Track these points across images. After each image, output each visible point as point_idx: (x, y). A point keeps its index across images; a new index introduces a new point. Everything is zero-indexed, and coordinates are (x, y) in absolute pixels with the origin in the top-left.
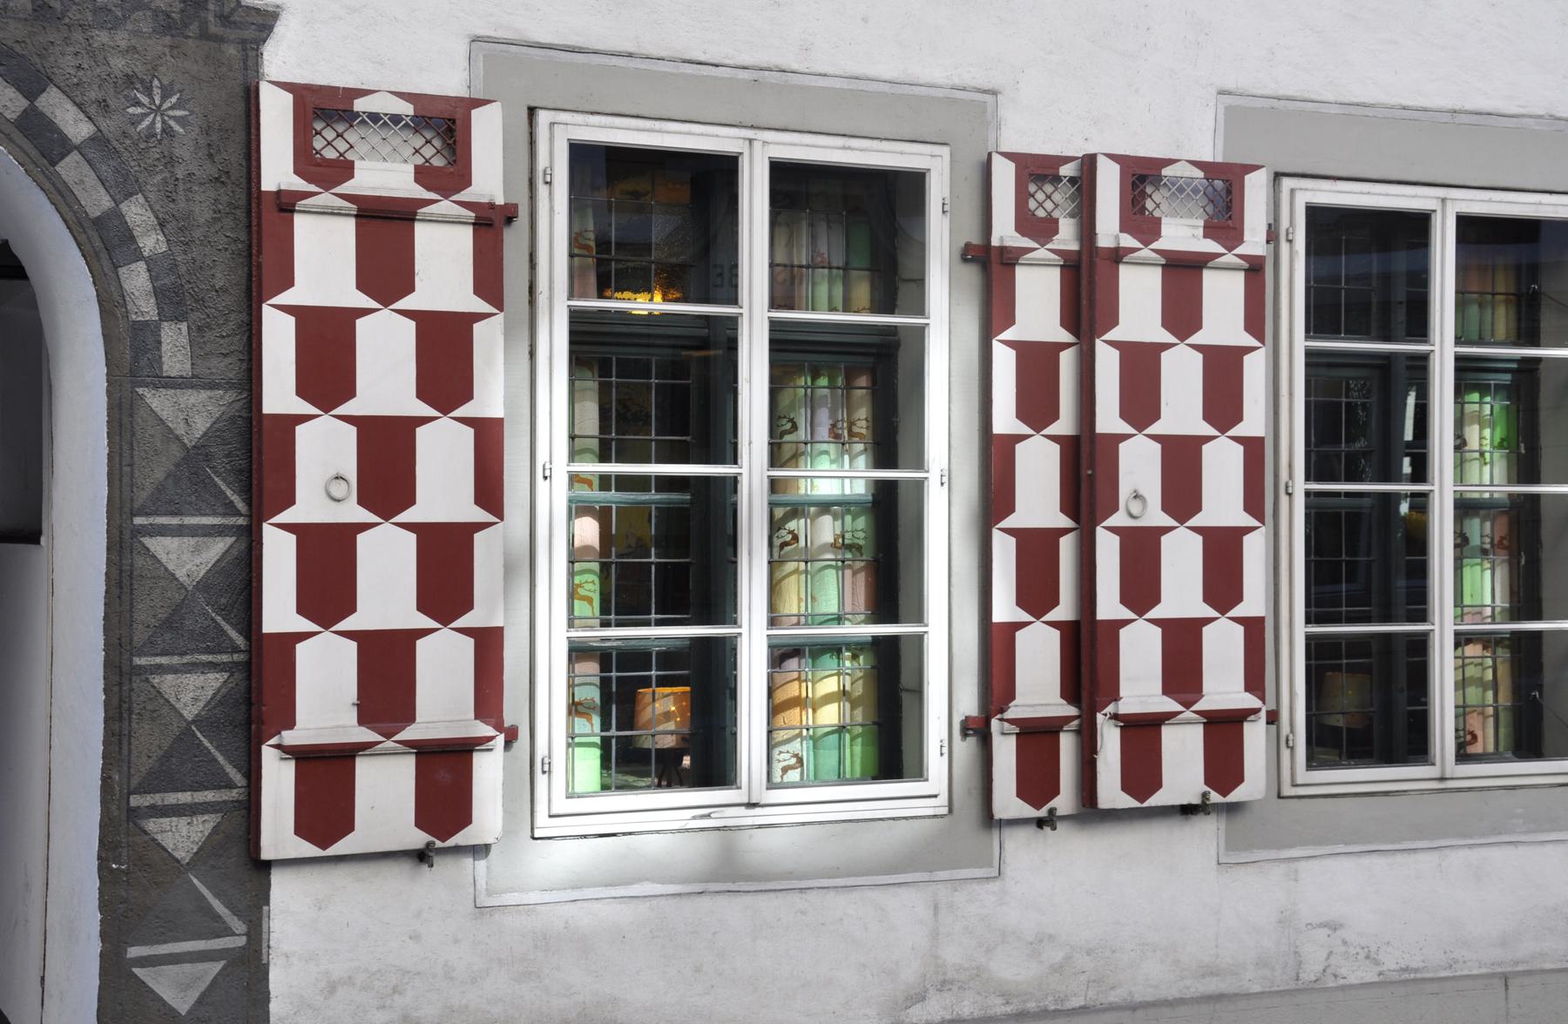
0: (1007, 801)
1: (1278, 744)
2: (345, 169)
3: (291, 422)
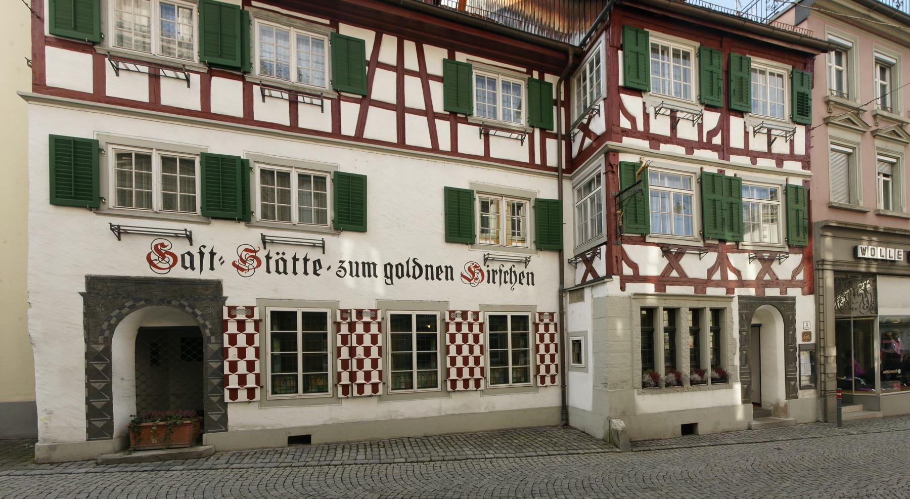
0: (539, 384)
1: (486, 382)
2: (235, 316)
3: (227, 348)
